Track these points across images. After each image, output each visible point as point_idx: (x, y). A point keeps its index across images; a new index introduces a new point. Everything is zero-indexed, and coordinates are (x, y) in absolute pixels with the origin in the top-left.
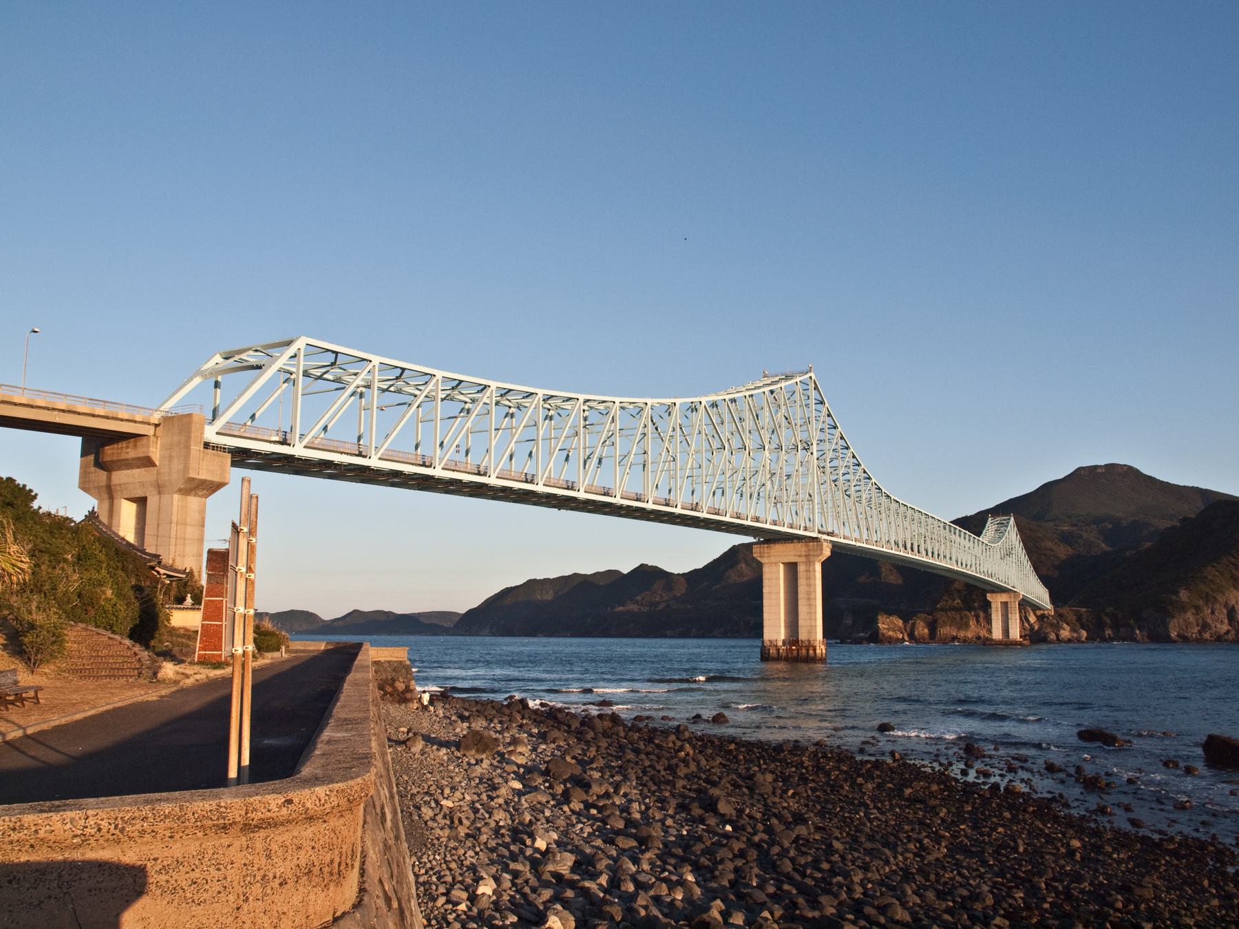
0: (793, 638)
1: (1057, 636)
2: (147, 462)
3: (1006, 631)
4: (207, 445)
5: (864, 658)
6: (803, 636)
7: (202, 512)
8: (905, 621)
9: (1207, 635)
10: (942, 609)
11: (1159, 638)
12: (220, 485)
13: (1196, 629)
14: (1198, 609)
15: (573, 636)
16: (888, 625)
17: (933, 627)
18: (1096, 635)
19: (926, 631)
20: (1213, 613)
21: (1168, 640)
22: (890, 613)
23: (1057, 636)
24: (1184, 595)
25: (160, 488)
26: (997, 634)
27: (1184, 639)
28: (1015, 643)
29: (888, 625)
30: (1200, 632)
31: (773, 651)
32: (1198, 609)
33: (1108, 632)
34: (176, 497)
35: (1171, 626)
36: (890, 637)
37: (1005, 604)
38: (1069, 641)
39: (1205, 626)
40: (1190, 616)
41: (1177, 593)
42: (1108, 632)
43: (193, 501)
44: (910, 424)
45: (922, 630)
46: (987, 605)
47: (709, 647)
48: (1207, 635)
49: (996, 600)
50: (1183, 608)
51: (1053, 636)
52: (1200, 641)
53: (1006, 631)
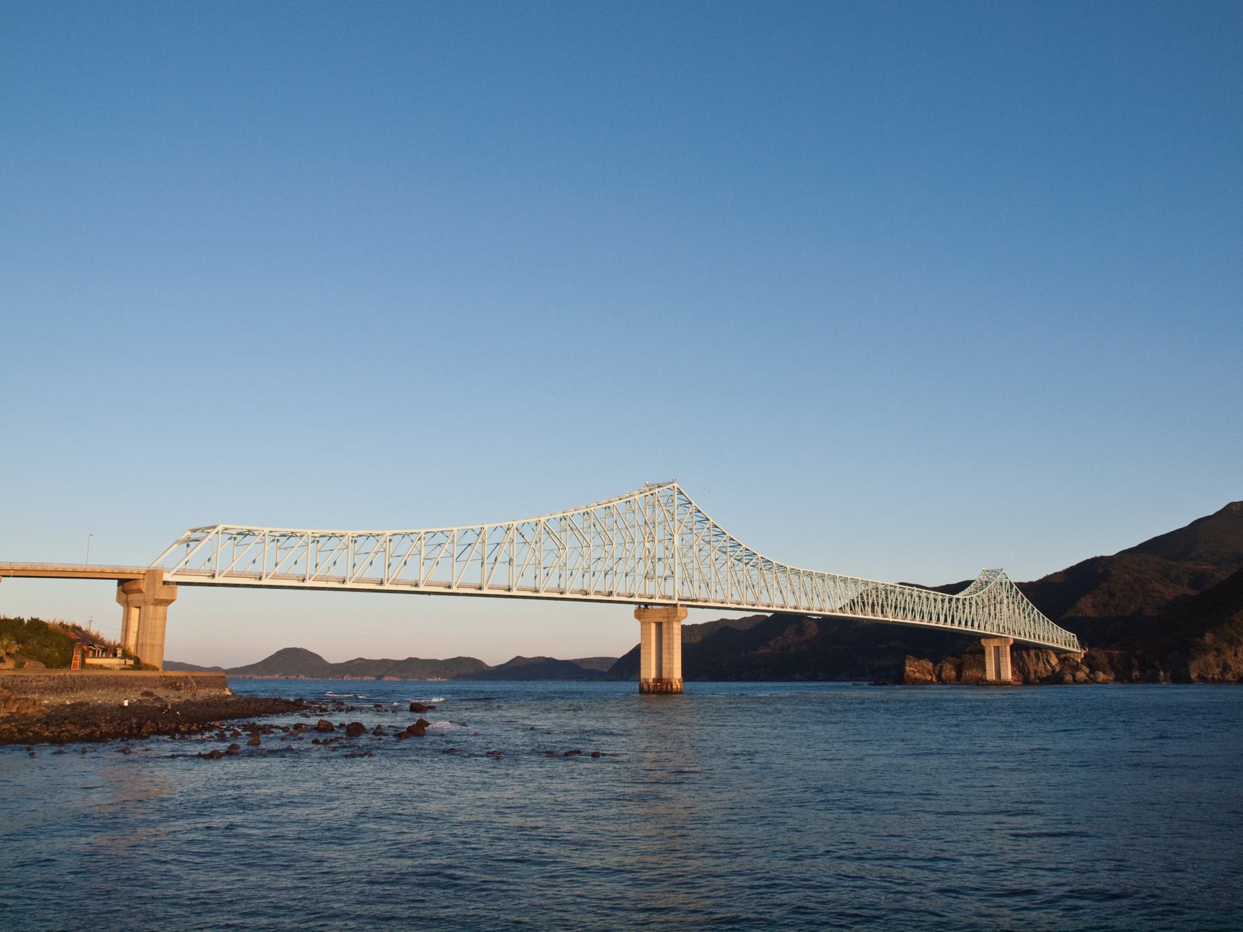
0: (659, 679)
1: (1074, 676)
2: (140, 591)
3: (998, 672)
4: (165, 583)
5: (845, 693)
6: (665, 676)
7: (165, 613)
8: (935, 665)
9: (1229, 676)
10: (970, 653)
11: (1180, 678)
12: (172, 601)
13: (1217, 671)
14: (1219, 651)
15: (711, 680)
16: (912, 668)
17: (959, 670)
18: (1123, 676)
19: (953, 673)
20: (1236, 655)
21: (1189, 681)
22: (919, 656)
23: (1074, 676)
24: (1208, 638)
25: (145, 603)
26: (991, 675)
27: (1203, 679)
28: (1007, 684)
29: (912, 668)
30: (1222, 673)
31: (645, 686)
32: (1219, 651)
33: (1136, 673)
34: (151, 607)
35: (1192, 667)
36: (916, 679)
37: (997, 649)
38: (1085, 682)
39: (1226, 668)
40: (1211, 659)
41: (1202, 636)
42: (1136, 673)
43: (160, 609)
44: (957, 491)
45: (949, 672)
46: (982, 652)
47: (742, 689)
48: (1229, 676)
49: (989, 647)
50: (1204, 651)
51: (1069, 677)
52: (1222, 681)
53: (998, 672)
